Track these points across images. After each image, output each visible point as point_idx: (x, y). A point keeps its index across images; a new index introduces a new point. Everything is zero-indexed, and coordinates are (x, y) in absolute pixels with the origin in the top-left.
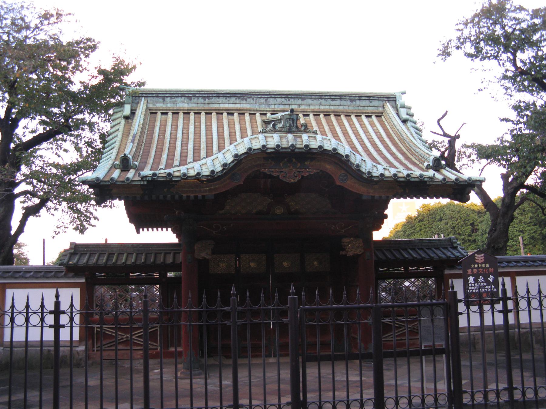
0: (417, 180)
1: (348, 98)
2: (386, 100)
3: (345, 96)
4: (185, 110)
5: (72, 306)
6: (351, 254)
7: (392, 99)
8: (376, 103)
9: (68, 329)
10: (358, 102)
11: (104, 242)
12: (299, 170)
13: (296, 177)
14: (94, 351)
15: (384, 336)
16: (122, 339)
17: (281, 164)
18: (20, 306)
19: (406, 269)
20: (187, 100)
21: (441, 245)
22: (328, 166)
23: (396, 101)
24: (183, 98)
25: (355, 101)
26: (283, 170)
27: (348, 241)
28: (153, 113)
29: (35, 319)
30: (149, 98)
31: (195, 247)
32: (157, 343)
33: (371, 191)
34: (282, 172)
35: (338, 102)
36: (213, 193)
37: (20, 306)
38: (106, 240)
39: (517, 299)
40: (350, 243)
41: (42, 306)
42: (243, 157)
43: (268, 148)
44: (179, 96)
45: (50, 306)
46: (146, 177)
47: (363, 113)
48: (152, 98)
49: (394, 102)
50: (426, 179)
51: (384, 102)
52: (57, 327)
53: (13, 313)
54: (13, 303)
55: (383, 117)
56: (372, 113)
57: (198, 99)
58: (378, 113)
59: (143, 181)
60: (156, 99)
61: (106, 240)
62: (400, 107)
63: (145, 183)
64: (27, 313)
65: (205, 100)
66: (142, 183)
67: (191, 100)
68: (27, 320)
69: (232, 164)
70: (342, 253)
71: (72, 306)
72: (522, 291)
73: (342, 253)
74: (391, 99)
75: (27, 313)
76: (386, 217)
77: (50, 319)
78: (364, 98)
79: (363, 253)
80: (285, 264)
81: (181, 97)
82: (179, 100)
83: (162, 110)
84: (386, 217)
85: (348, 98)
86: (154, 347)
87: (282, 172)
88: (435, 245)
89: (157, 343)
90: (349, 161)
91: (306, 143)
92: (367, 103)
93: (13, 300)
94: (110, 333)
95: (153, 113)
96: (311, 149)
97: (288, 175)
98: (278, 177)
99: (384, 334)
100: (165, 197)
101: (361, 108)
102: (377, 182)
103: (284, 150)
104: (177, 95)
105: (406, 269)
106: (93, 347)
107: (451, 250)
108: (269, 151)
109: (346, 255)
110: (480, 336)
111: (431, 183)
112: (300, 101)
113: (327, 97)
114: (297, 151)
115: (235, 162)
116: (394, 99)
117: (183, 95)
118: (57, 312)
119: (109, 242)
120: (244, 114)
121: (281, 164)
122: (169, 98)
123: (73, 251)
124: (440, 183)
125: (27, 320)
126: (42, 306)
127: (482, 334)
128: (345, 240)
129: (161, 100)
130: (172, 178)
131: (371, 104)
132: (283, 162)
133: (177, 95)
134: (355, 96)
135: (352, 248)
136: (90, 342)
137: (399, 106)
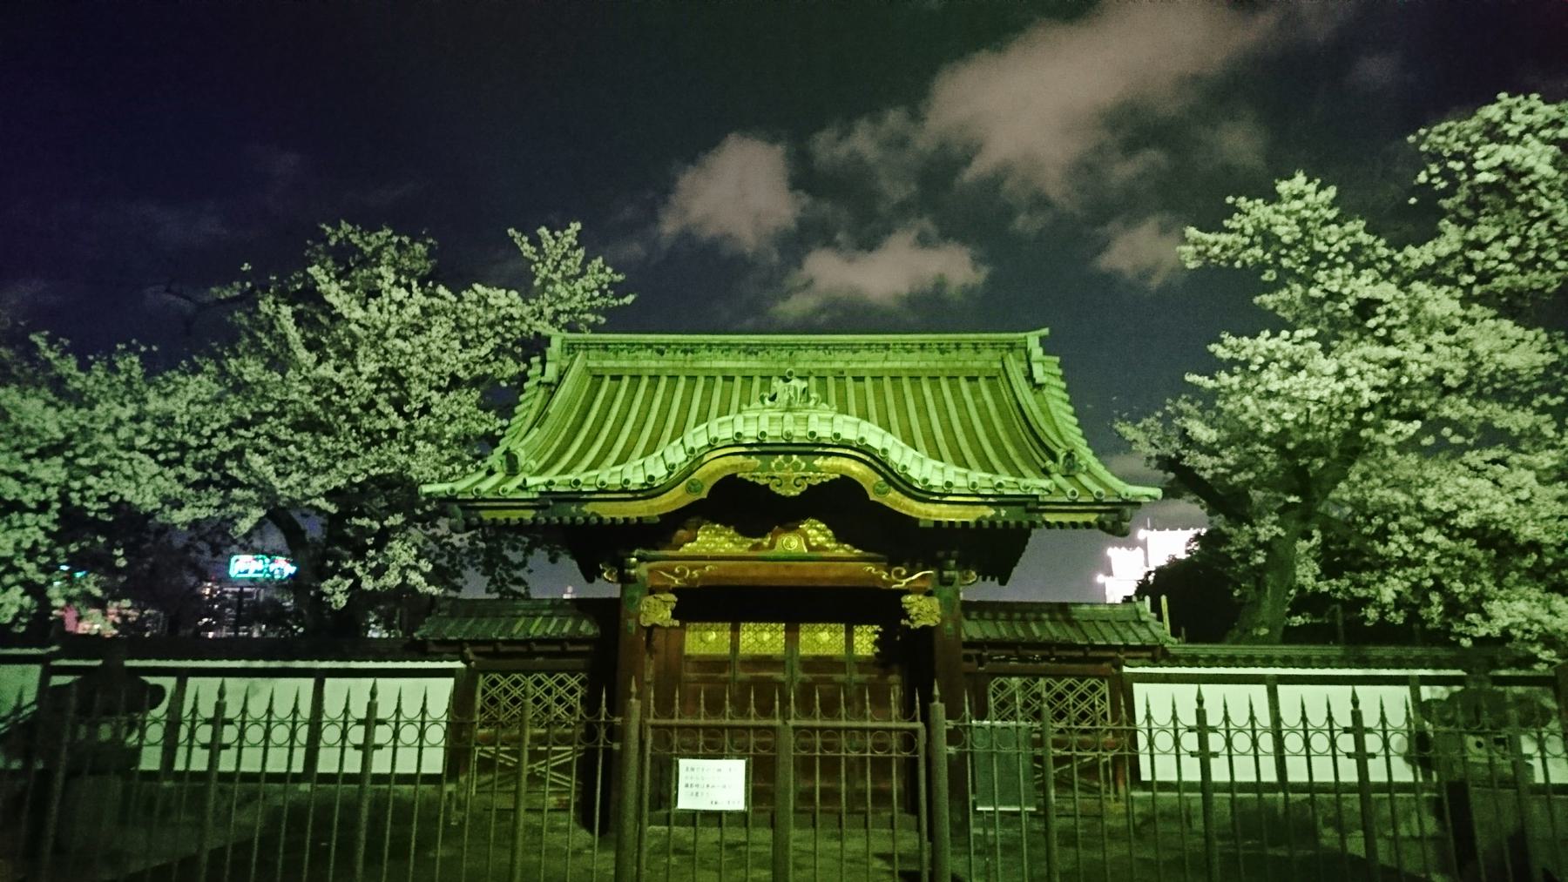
5: (295, 711)
9: (1381, 760)
18: (1162, 717)
28: (598, 378)
29: (1320, 742)
35: (917, 355)
37: (1162, 717)
39: (1280, 732)
41: (346, 711)
45: (1344, 719)
52: (1204, 755)
53: (193, 722)
54: (195, 704)
64: (269, 722)
68: (422, 734)
71: (295, 711)
72: (1290, 717)
75: (269, 722)
77: (1190, 742)
82: (641, 354)
93: (196, 698)
95: (598, 378)
98: (767, 486)
100: (573, 519)
110: (1200, 802)
112: (849, 355)
118: (1358, 729)
120: (918, 378)
125: (422, 734)
126: (346, 711)
127: (1207, 800)
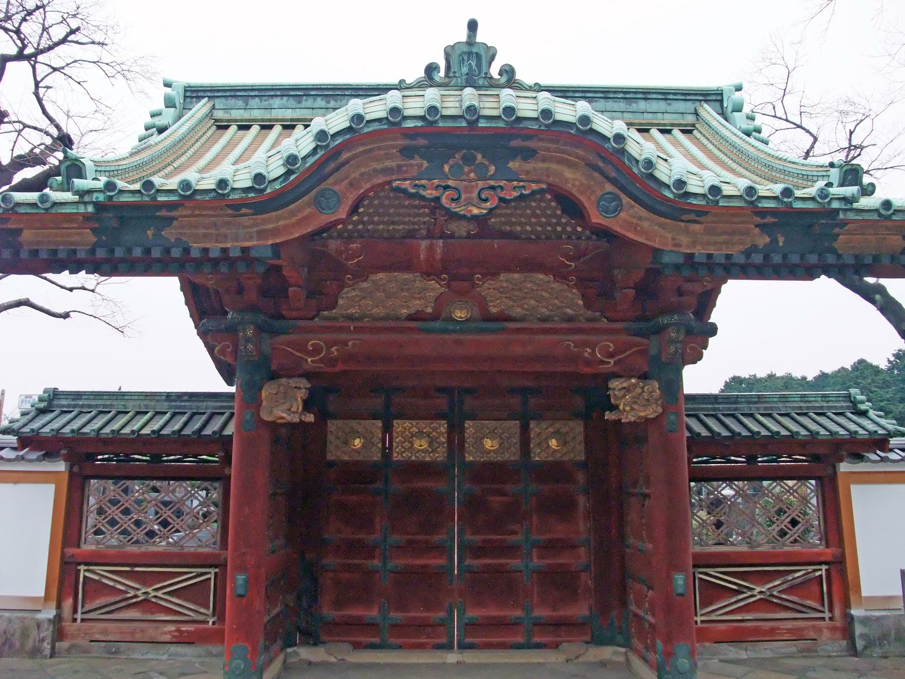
0: (810, 205)
1: (621, 95)
2: (700, 101)
3: (615, 92)
4: (287, 120)
6: (629, 417)
7: (714, 98)
8: (681, 106)
10: (642, 105)
11: (117, 390)
12: (492, 183)
13: (486, 200)
14: (75, 620)
15: (704, 611)
16: (136, 596)
17: (446, 168)
19: (751, 459)
20: (292, 102)
21: (829, 408)
22: (568, 174)
23: (721, 101)
24: (285, 99)
25: (636, 103)
26: (450, 183)
27: (625, 385)
30: (217, 101)
31: (263, 394)
32: (208, 608)
33: (684, 239)
34: (446, 187)
36: (270, 242)
38: (120, 389)
40: (628, 390)
42: (339, 140)
43: (405, 118)
44: (276, 96)
46: (90, 192)
47: (653, 125)
48: (223, 100)
49: (718, 104)
50: (835, 205)
51: (698, 104)
55: (695, 132)
56: (673, 125)
57: (314, 101)
58: (686, 125)
59: (85, 203)
60: (232, 102)
61: (120, 389)
62: (733, 111)
63: (90, 209)
65: (328, 102)
66: (82, 209)
67: (299, 102)
69: (311, 160)
70: (608, 416)
73: (608, 416)
74: (714, 97)
76: (713, 330)
78: (654, 96)
79: (663, 413)
80: (488, 444)
81: (282, 96)
82: (277, 102)
83: (242, 121)
84: (713, 330)
85: (621, 95)
86: (201, 618)
87: (446, 187)
88: (815, 408)
89: (208, 608)
90: (623, 151)
91: (508, 104)
92: (661, 106)
94: (111, 583)
96: (520, 119)
97: (463, 196)
99: (704, 605)
101: (650, 116)
102: (701, 212)
103: (450, 124)
104: (272, 93)
105: (751, 459)
106: (75, 611)
107: (854, 418)
108: (409, 124)
109: (620, 420)
111: (851, 216)
113: (577, 95)
114: (482, 124)
115: (321, 153)
116: (719, 98)
117: (285, 93)
119: (122, 390)
121: (446, 168)
122: (257, 100)
123: (42, 405)
124: (875, 217)
128: (615, 384)
129: (240, 103)
130: (154, 198)
131: (669, 109)
132: (451, 162)
133: (272, 93)
134: (636, 93)
135: (632, 402)
136: (68, 603)
137: (730, 109)
